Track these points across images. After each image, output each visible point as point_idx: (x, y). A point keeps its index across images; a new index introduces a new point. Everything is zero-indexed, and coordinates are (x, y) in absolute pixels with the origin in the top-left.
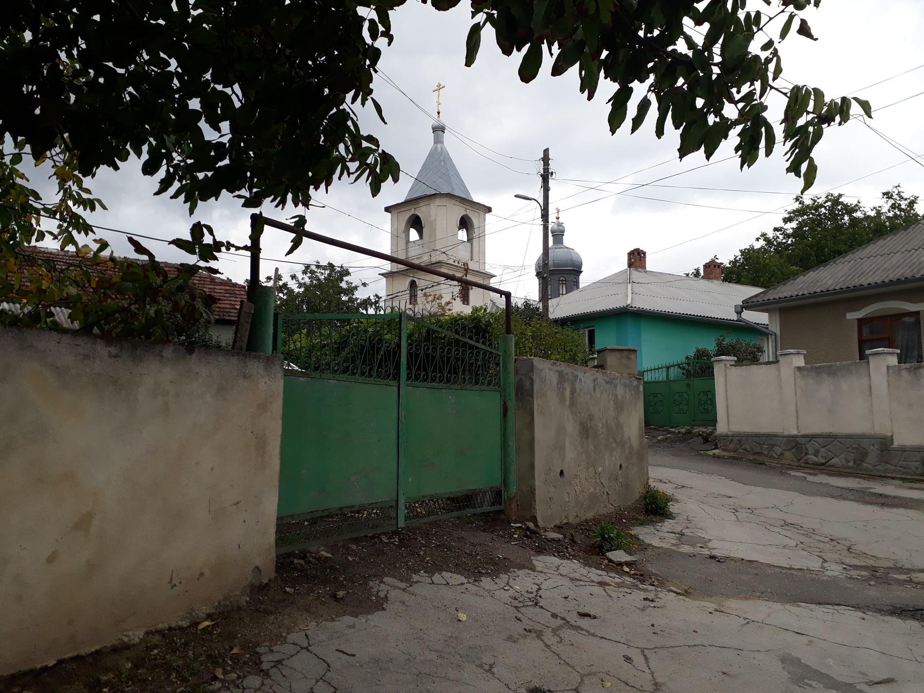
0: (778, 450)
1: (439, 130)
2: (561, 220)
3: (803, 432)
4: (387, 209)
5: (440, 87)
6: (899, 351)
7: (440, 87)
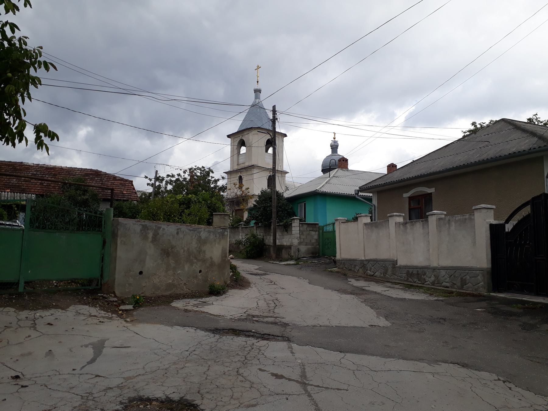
0: (357, 268)
1: (257, 91)
2: (336, 140)
3: (367, 258)
4: (229, 136)
5: (258, 67)
6: (404, 215)
7: (258, 67)
